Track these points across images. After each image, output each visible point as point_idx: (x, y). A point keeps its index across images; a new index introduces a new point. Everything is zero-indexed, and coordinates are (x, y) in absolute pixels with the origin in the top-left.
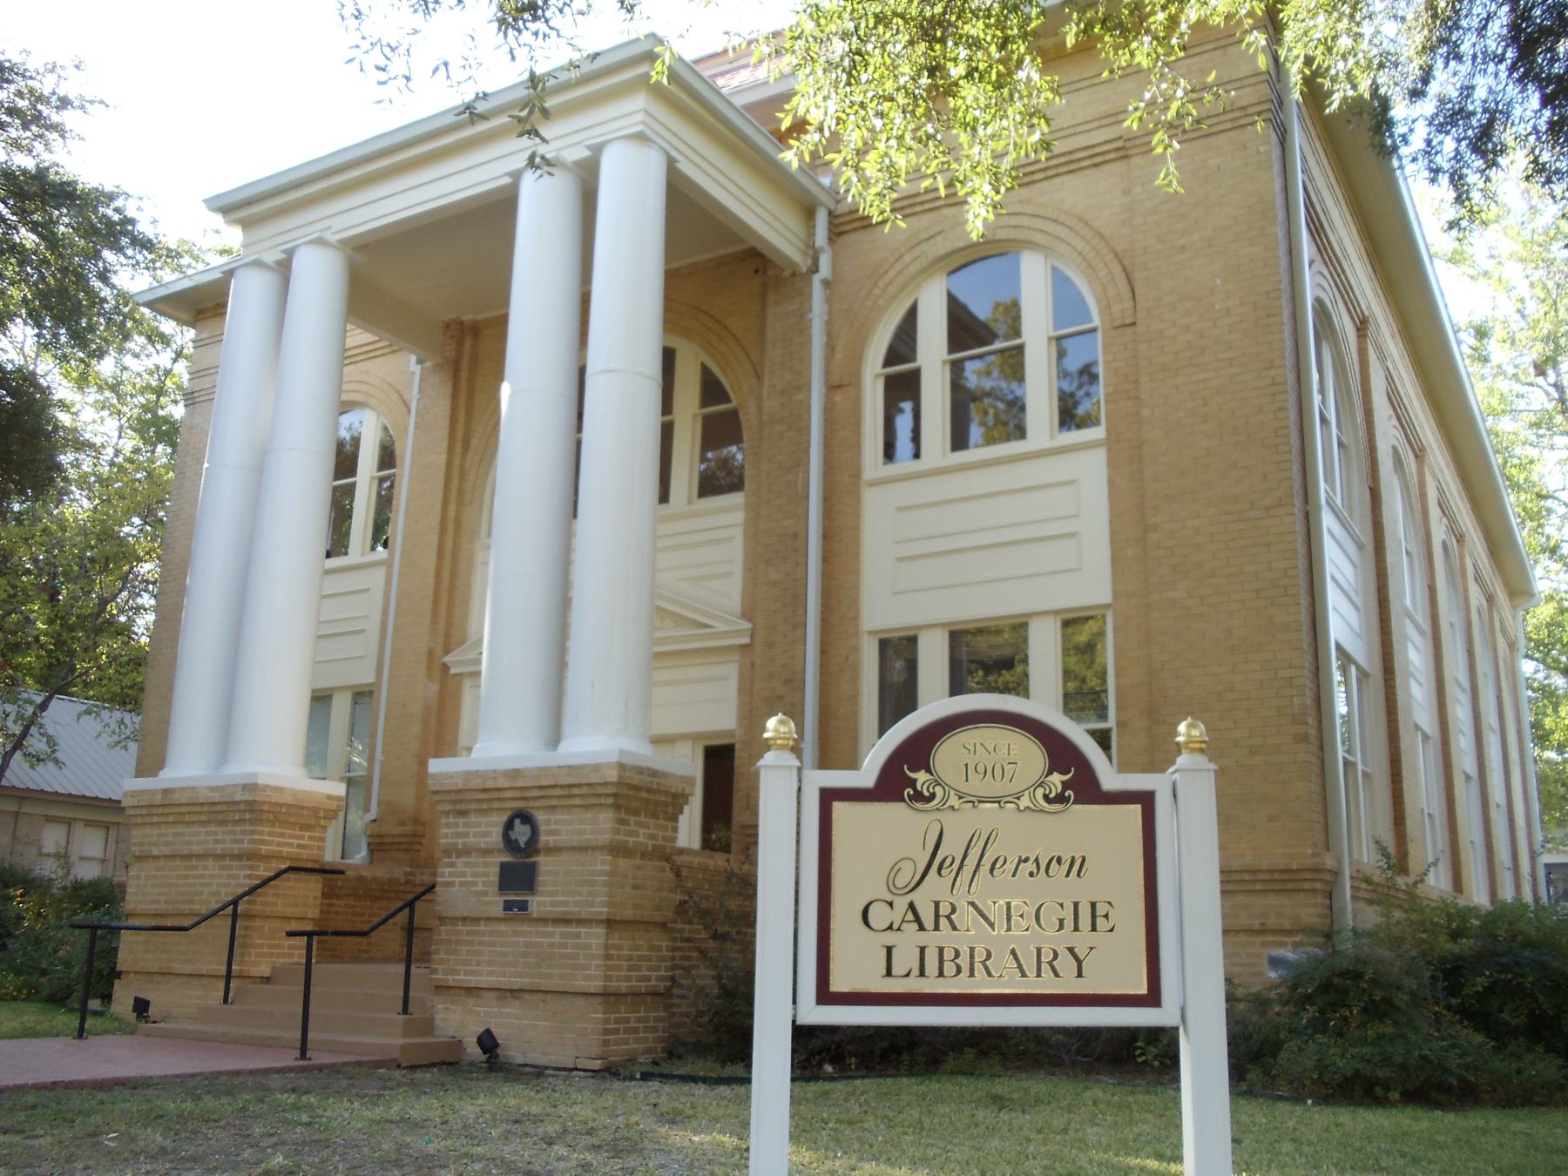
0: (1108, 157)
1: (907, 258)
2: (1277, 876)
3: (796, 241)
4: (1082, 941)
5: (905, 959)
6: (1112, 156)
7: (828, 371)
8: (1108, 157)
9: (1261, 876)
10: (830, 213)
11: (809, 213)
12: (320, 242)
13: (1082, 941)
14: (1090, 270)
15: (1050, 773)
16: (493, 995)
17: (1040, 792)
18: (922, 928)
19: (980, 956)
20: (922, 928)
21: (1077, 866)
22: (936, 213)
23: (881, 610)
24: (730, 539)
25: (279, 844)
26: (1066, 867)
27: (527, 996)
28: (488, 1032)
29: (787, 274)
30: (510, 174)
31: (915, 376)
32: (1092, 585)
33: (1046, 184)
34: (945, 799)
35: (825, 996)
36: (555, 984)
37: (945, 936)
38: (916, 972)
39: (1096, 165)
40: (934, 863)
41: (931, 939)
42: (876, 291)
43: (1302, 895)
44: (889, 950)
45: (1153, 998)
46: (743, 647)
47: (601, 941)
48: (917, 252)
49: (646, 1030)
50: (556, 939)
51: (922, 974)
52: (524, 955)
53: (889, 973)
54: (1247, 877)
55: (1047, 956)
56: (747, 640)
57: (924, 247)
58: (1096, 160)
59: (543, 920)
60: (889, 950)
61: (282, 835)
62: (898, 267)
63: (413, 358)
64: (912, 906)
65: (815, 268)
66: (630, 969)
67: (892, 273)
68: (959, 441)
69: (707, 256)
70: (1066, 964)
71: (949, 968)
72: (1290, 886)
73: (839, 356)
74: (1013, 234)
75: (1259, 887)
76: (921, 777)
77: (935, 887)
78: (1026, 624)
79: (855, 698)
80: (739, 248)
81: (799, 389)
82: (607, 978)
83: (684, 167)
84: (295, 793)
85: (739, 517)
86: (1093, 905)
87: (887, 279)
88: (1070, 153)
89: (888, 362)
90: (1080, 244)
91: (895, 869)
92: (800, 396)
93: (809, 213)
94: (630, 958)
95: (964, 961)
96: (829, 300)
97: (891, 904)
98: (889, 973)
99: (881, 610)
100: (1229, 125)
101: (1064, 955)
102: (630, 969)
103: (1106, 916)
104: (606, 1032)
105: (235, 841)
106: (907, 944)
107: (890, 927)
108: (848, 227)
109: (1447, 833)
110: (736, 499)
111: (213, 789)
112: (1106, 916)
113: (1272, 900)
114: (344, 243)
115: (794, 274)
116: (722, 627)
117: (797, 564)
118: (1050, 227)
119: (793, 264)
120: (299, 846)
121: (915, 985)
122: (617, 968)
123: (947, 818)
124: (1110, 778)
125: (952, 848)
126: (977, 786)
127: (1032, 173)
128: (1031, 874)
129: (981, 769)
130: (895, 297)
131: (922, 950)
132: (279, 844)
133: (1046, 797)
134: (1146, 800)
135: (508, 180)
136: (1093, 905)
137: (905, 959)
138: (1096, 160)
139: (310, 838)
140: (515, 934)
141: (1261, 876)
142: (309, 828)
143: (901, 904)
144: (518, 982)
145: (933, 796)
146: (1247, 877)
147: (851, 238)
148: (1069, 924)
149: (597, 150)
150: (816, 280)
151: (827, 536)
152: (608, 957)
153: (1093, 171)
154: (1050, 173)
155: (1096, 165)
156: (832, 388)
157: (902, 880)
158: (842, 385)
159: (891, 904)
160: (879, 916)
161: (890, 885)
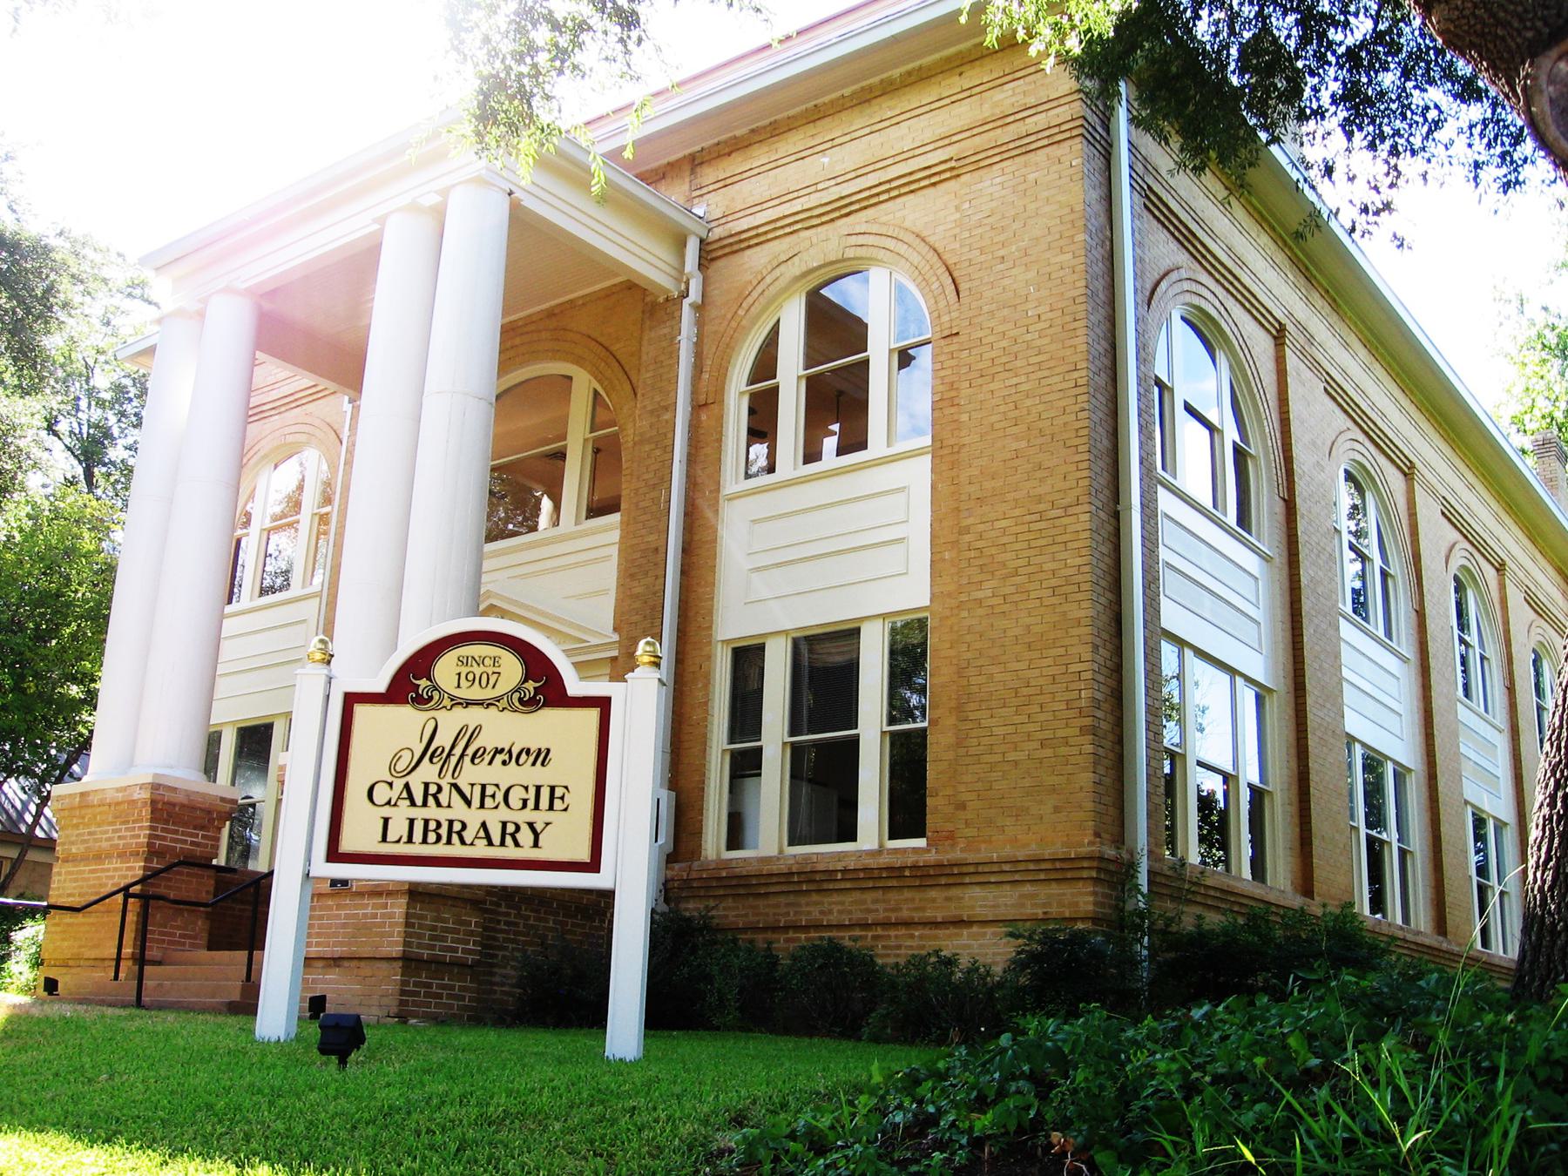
0: (944, 176)
1: (768, 280)
2: (1058, 865)
3: (668, 269)
4: (539, 818)
5: (398, 829)
6: (948, 175)
7: (694, 392)
8: (944, 176)
9: (1044, 866)
10: (702, 241)
11: (680, 243)
12: (228, 290)
13: (539, 818)
14: (923, 283)
15: (526, 681)
16: (320, 964)
17: (516, 695)
18: (413, 804)
19: (457, 827)
20: (413, 804)
21: (542, 757)
22: (795, 236)
23: (733, 621)
24: (607, 558)
25: (173, 840)
26: (532, 759)
27: (346, 964)
28: (323, 998)
29: (661, 300)
30: (375, 221)
31: (774, 392)
32: (912, 591)
33: (890, 204)
34: (441, 700)
35: (334, 855)
36: (366, 951)
37: (432, 812)
38: (405, 839)
39: (934, 184)
40: (429, 752)
41: (419, 813)
42: (741, 312)
43: (1081, 884)
44: (386, 820)
45: (593, 866)
46: (614, 659)
47: (403, 910)
48: (777, 272)
49: (450, 996)
50: (369, 911)
51: (410, 840)
52: (344, 926)
53: (384, 839)
54: (1031, 866)
55: (511, 828)
56: (615, 653)
57: (782, 268)
58: (934, 180)
59: (360, 894)
60: (386, 820)
61: (176, 832)
62: (759, 289)
63: (346, 398)
64: (407, 786)
65: (685, 295)
66: (432, 938)
67: (755, 294)
68: (812, 454)
69: (597, 287)
70: (525, 836)
71: (432, 837)
72: (1069, 875)
73: (706, 376)
74: (860, 252)
75: (1042, 876)
76: (423, 683)
77: (428, 772)
78: (858, 630)
79: (706, 704)
80: (620, 279)
81: (666, 408)
82: (406, 944)
83: (529, 203)
84: (188, 793)
85: (615, 536)
86: (552, 789)
87: (750, 300)
88: (911, 174)
89: (751, 382)
90: (916, 259)
91: (397, 757)
92: (667, 416)
93: (680, 243)
94: (434, 928)
95: (444, 831)
96: (700, 324)
97: (391, 784)
98: (384, 839)
99: (733, 621)
100: (1045, 142)
101: (525, 829)
102: (432, 938)
103: (562, 798)
104: (403, 993)
105: (133, 837)
106: (400, 816)
107: (389, 803)
108: (720, 253)
109: (1429, 867)
110: (615, 518)
111: (118, 790)
112: (562, 798)
113: (1054, 889)
114: (249, 292)
115: (667, 300)
116: (594, 641)
117: (657, 577)
118: (890, 243)
119: (667, 291)
120: (192, 843)
121: (403, 849)
122: (420, 936)
123: (441, 715)
124: (575, 686)
125: (444, 740)
126: (466, 693)
127: (878, 194)
128: (504, 763)
129: (471, 677)
130: (758, 316)
131: (412, 821)
132: (173, 840)
133: (520, 700)
134: (603, 704)
135: (376, 227)
136: (552, 789)
137: (398, 829)
138: (934, 180)
139: (204, 837)
140: (339, 907)
141: (1044, 866)
142: (202, 828)
143: (399, 785)
144: (338, 951)
145: (431, 698)
146: (1031, 866)
147: (720, 263)
148: (531, 804)
149: (445, 193)
150: (686, 302)
151: (687, 550)
152: (407, 924)
153: (931, 190)
154: (893, 194)
155: (934, 184)
156: (698, 407)
157: (401, 766)
158: (706, 404)
159: (391, 784)
160: (381, 794)
161: (392, 767)
